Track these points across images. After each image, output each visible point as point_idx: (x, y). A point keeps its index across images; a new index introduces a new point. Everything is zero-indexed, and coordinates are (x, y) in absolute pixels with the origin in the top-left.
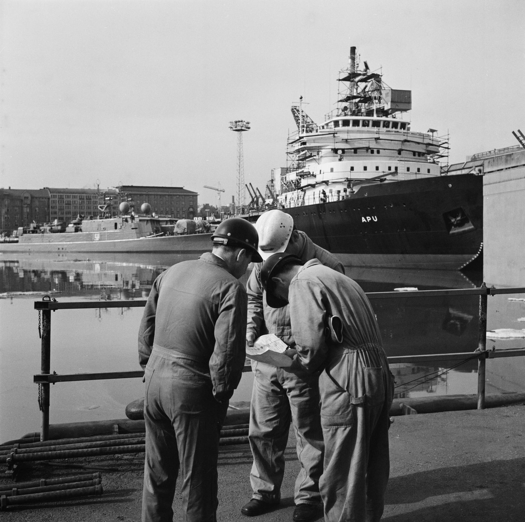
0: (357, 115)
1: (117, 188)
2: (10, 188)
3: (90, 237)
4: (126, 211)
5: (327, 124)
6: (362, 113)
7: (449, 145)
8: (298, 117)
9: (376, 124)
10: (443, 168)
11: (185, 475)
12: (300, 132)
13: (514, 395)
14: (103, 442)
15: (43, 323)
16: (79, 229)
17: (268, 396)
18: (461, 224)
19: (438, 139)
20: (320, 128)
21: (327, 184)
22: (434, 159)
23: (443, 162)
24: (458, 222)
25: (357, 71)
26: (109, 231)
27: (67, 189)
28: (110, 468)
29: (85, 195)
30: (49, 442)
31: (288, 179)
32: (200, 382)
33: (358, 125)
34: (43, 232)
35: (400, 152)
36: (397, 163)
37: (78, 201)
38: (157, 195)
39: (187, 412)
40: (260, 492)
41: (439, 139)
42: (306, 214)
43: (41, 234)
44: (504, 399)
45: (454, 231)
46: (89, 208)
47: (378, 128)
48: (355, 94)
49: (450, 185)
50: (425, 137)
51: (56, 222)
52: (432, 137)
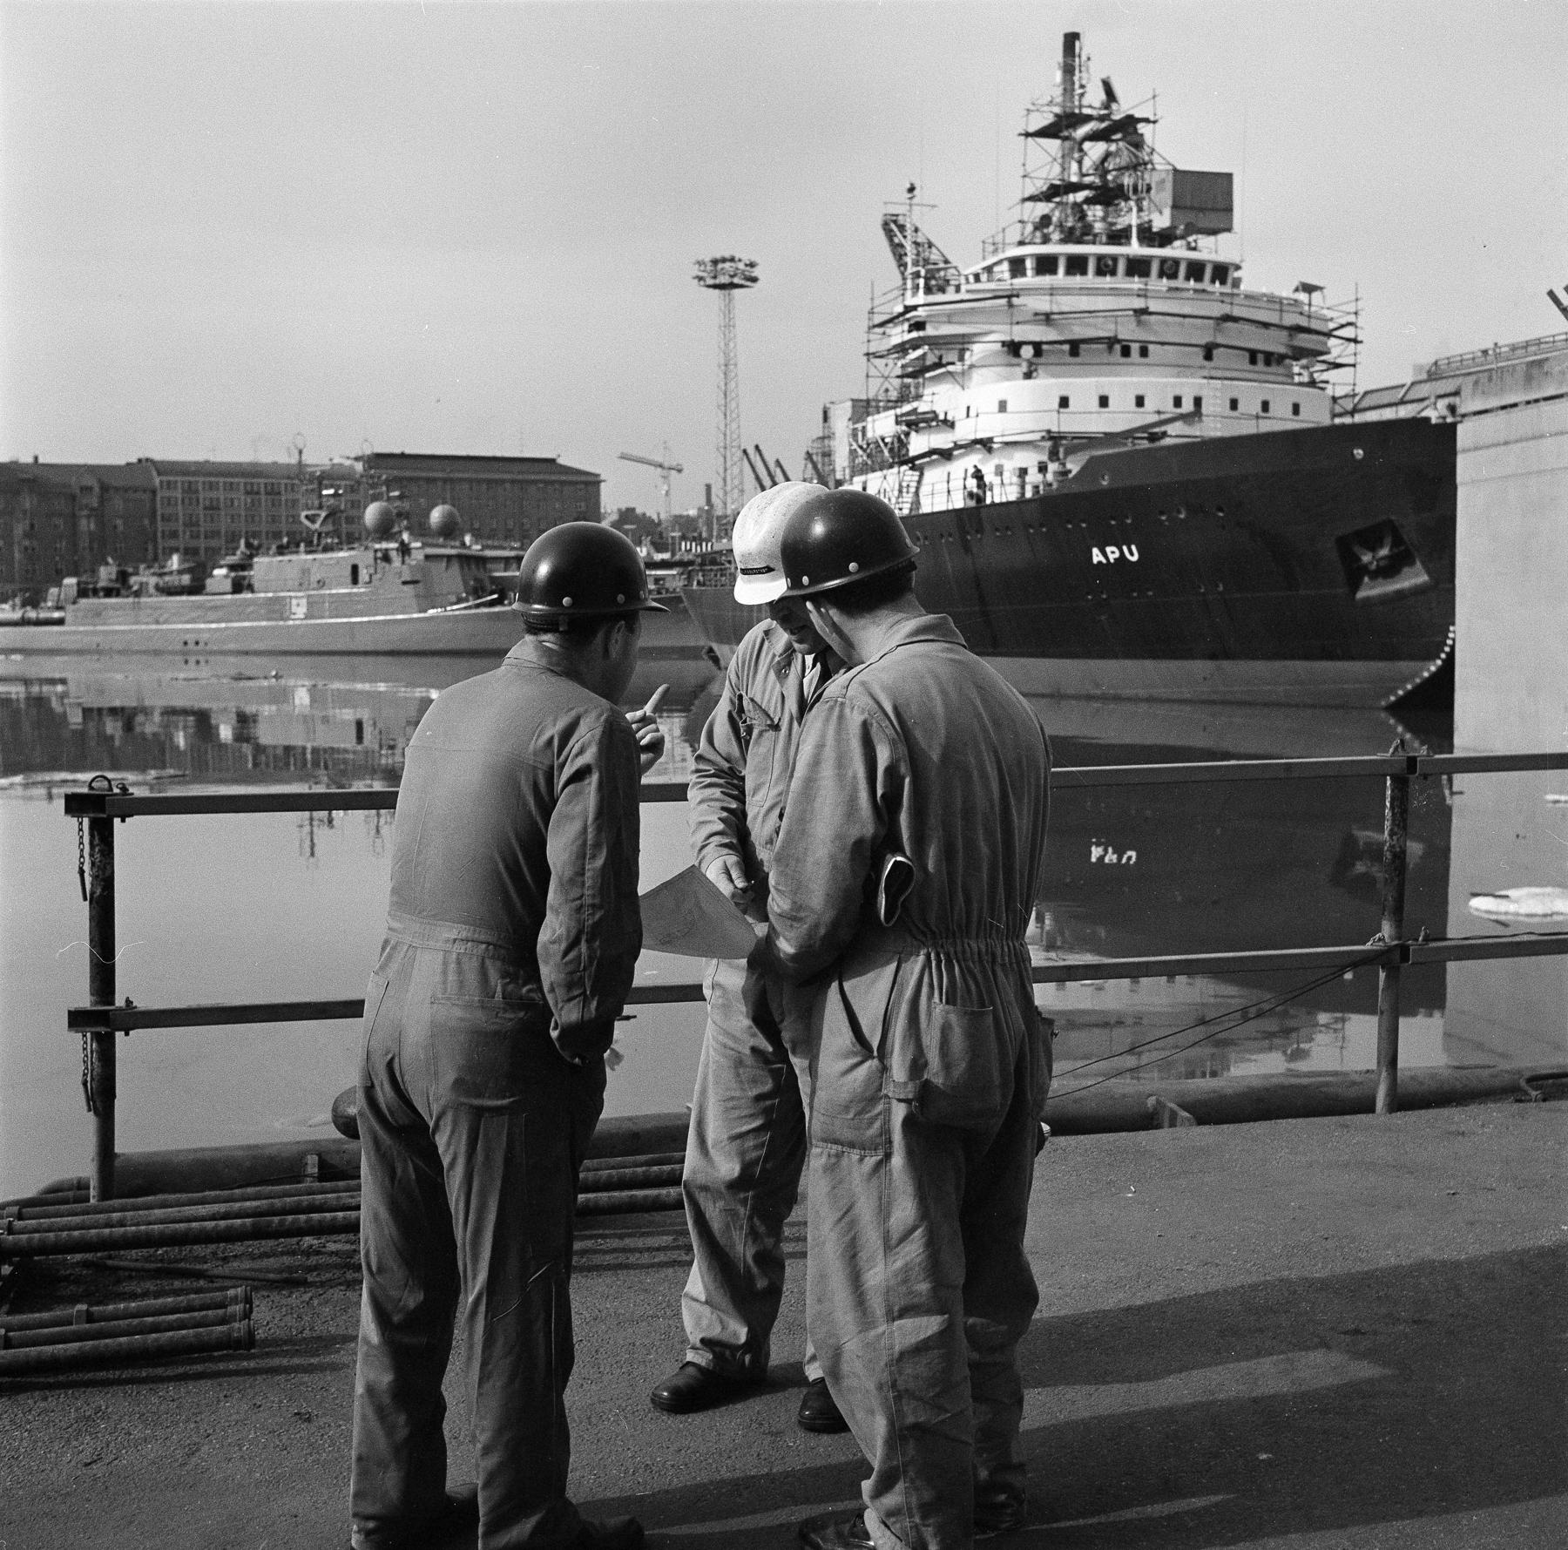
0: (1079, 242)
1: (357, 459)
2: (36, 458)
3: (277, 609)
4: (385, 530)
5: (989, 269)
6: (1095, 235)
7: (1359, 331)
8: (902, 246)
9: (1138, 267)
10: (1340, 401)
11: (470, 1283)
12: (909, 293)
13: (1487, 1072)
14: (264, 1202)
15: (91, 855)
16: (246, 582)
17: (739, 1063)
18: (1390, 569)
19: (1325, 312)
20: (967, 279)
21: (990, 450)
22: (1311, 374)
23: (1339, 383)
24: (1382, 563)
25: (1081, 107)
26: (334, 591)
27: (207, 462)
28: (285, 1275)
29: (262, 481)
30: (116, 1202)
31: (870, 434)
32: (508, 1015)
33: (1084, 272)
34: (137, 594)
35: (1209, 351)
36: (1201, 386)
37: (241, 498)
38: (479, 481)
39: (477, 1102)
40: (707, 1343)
41: (1329, 314)
42: (926, 538)
43: (131, 600)
44: (1459, 1085)
45: (1370, 590)
46: (274, 519)
47: (1143, 280)
48: (1074, 179)
49: (1359, 453)
50: (1285, 308)
51: (175, 562)
52: (1306, 308)
